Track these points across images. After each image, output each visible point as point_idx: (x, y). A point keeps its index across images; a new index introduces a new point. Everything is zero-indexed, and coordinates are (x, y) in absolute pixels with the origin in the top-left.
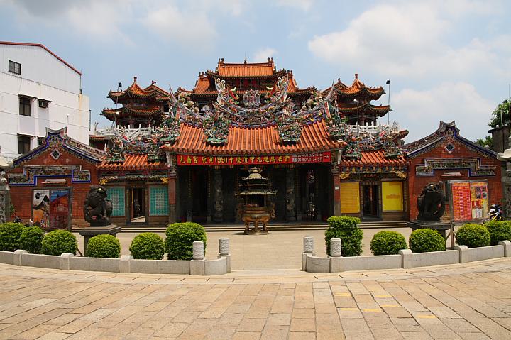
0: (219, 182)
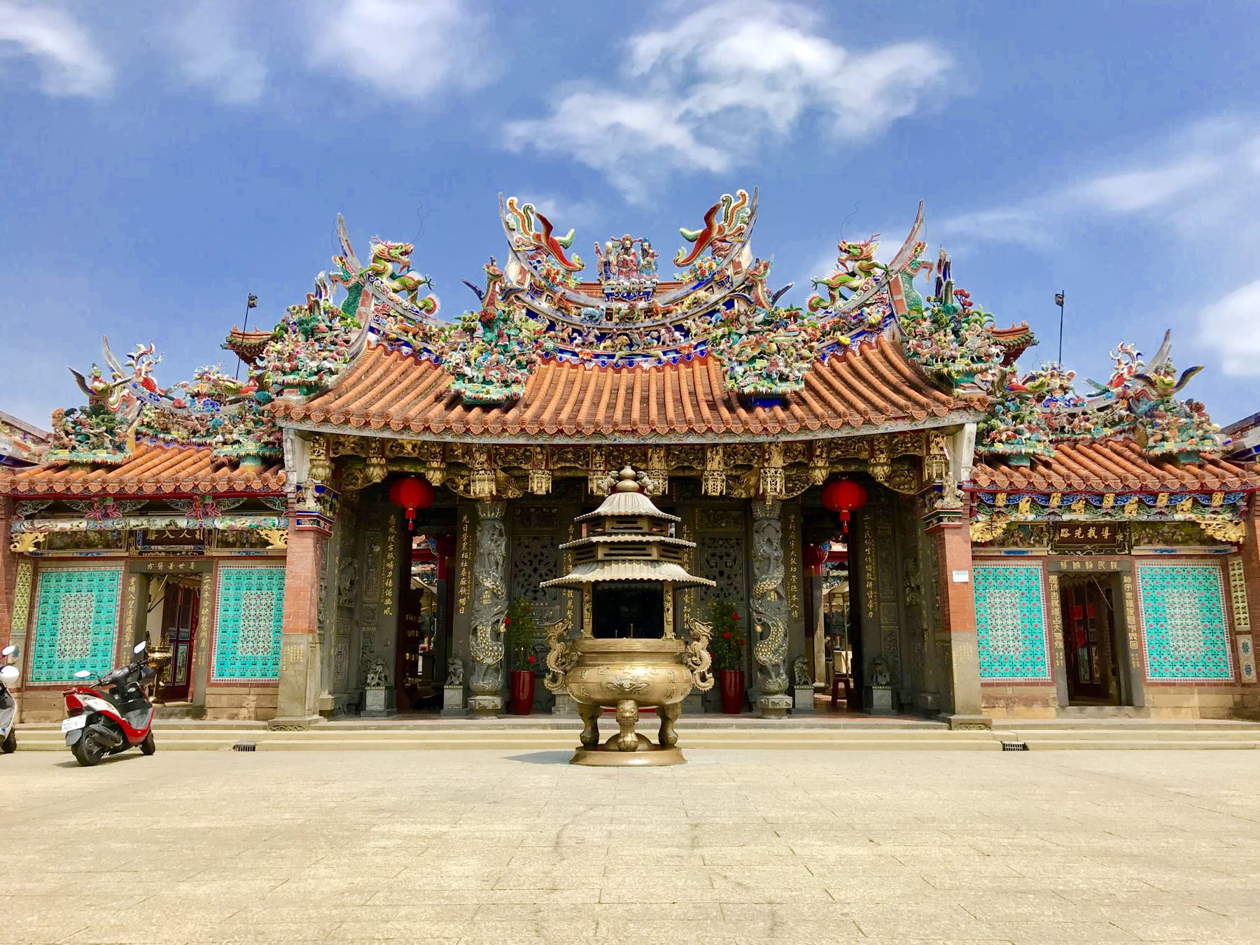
0: (493, 546)
